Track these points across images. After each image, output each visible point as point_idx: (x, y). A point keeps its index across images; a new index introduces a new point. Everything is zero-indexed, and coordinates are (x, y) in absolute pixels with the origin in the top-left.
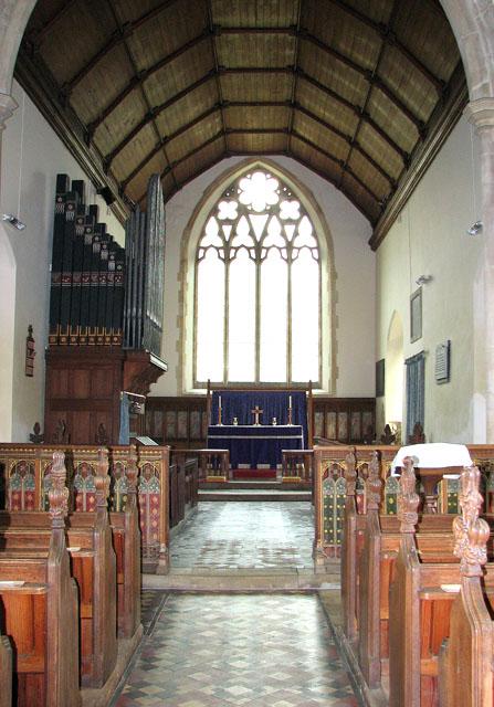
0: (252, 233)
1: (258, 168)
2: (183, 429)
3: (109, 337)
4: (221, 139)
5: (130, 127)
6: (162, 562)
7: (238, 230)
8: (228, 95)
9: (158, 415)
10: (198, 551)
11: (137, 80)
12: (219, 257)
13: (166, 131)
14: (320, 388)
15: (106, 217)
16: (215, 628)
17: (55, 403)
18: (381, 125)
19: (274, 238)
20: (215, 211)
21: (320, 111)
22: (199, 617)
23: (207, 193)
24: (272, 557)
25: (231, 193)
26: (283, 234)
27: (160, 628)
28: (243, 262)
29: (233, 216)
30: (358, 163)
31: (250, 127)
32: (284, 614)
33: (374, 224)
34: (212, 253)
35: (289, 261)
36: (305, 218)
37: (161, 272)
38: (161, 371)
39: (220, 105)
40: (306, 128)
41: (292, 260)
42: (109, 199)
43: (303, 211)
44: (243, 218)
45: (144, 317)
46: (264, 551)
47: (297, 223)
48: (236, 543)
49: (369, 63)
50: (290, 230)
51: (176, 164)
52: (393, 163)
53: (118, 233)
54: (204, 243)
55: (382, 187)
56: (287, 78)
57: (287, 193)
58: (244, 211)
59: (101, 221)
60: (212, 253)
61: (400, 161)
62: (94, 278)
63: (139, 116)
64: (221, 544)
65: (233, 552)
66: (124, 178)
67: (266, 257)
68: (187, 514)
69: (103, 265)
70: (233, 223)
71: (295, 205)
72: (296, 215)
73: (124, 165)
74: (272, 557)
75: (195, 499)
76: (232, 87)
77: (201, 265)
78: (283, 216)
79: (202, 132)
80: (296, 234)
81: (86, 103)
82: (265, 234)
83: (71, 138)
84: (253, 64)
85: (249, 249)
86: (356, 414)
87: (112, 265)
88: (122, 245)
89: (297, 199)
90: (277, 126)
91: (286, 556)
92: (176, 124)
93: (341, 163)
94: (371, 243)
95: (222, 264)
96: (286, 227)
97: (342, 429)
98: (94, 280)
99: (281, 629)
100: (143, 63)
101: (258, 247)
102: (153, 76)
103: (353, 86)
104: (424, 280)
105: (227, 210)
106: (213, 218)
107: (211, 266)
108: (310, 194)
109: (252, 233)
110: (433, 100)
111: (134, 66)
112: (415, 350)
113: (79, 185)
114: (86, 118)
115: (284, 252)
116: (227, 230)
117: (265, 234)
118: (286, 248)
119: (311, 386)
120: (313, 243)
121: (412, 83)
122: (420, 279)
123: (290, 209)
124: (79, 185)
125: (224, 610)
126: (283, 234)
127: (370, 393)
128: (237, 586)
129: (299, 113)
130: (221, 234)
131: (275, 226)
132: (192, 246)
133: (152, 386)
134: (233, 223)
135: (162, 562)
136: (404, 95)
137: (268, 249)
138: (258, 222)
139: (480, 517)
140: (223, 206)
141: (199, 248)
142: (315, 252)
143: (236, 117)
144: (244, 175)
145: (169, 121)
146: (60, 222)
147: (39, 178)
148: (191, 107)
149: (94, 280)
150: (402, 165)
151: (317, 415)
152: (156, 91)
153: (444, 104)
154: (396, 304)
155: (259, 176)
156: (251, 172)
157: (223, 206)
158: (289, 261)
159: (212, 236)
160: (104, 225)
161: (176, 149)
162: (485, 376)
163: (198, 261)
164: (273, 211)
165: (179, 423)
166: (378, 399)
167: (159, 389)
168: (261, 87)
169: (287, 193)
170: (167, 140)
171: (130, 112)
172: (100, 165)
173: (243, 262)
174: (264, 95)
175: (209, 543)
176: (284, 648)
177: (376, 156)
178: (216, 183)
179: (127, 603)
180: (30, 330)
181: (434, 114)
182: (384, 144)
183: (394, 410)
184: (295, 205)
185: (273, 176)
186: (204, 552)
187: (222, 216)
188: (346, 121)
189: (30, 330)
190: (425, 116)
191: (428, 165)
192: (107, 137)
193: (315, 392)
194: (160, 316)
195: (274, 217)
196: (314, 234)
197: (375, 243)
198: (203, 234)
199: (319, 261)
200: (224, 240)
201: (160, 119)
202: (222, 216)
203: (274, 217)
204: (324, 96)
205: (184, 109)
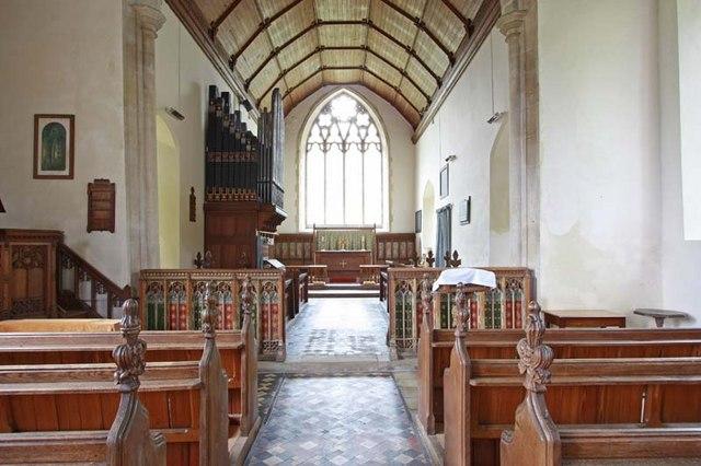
1: (343, 93)
2: (299, 253)
3: (249, 195)
4: (320, 73)
5: (261, 62)
6: (280, 353)
7: (331, 132)
8: (324, 42)
9: (285, 245)
10: (307, 338)
11: (264, 25)
13: (285, 66)
15: (245, 117)
16: (318, 413)
17: (209, 240)
18: (423, 58)
19: (354, 138)
20: (317, 120)
21: (383, 53)
22: (303, 395)
23: (312, 109)
24: (358, 345)
25: (326, 109)
26: (359, 135)
27: (275, 415)
28: (335, 151)
29: (328, 123)
30: (407, 88)
31: (338, 65)
32: (370, 398)
34: (316, 147)
36: (372, 125)
37: (280, 157)
38: (284, 218)
39: (320, 49)
40: (374, 65)
42: (248, 108)
43: (371, 120)
44: (334, 125)
45: (271, 182)
46: (352, 338)
47: (367, 128)
48: (333, 332)
49: (417, 13)
51: (292, 89)
52: (429, 85)
53: (253, 128)
54: (311, 140)
55: (420, 102)
56: (362, 28)
57: (361, 109)
58: (335, 120)
59: (242, 121)
60: (316, 147)
61: (435, 84)
62: (237, 156)
63: (267, 54)
64: (323, 332)
65: (331, 340)
66: (259, 97)
68: (301, 309)
69: (242, 148)
70: (329, 128)
71: (366, 116)
72: (367, 123)
73: (258, 88)
74: (358, 345)
75: (306, 297)
76: (327, 35)
77: (309, 154)
78: (359, 123)
79: (308, 68)
80: (367, 135)
81: (229, 42)
82: (348, 135)
83: (218, 61)
84: (340, 19)
86: (389, 243)
87: (248, 147)
88: (255, 134)
89: (366, 111)
90: (356, 65)
91: (368, 343)
92: (292, 61)
93: (395, 88)
94: (412, 139)
95: (322, 153)
97: (395, 252)
98: (237, 157)
99: (369, 415)
100: (267, 13)
102: (274, 23)
103: (406, 32)
104: (453, 158)
105: (325, 120)
106: (316, 125)
107: (315, 152)
108: (376, 110)
110: (462, 34)
111: (261, 15)
112: (440, 204)
113: (226, 95)
114: (231, 51)
115: (360, 146)
116: (325, 132)
117: (348, 135)
120: (377, 140)
121: (447, 23)
123: (363, 119)
124: (226, 95)
125: (324, 394)
129: (369, 54)
132: (303, 143)
133: (278, 227)
134: (329, 128)
135: (280, 353)
136: (439, 33)
138: (344, 128)
140: (322, 117)
141: (307, 144)
143: (330, 58)
144: (335, 97)
145: (287, 58)
146: (211, 117)
147: (196, 88)
148: (300, 49)
149: (237, 157)
150: (436, 86)
152: (277, 34)
153: (470, 36)
154: (428, 172)
155: (343, 98)
156: (338, 96)
157: (322, 117)
159: (316, 138)
160: (245, 124)
161: (292, 79)
162: (73, 327)
163: (307, 151)
164: (353, 120)
165: (297, 249)
166: (417, 235)
167: (281, 229)
168: (346, 36)
169: (361, 109)
170: (279, 50)
171: (259, 50)
172: (242, 87)
173: (335, 151)
174: (348, 42)
175: (315, 332)
176: (374, 438)
177: (419, 82)
178: (317, 102)
179: (246, 382)
180: (193, 190)
181: (462, 46)
182: (424, 72)
183: (428, 241)
184: (366, 116)
185: (353, 98)
186: (311, 340)
187: (321, 123)
188: (399, 57)
189: (193, 190)
190: (454, 48)
191: (455, 82)
192: (246, 66)
194: (281, 178)
196: (378, 135)
197: (415, 140)
198: (310, 135)
199: (381, 151)
201: (280, 56)
202: (321, 123)
204: (386, 40)
205: (296, 50)
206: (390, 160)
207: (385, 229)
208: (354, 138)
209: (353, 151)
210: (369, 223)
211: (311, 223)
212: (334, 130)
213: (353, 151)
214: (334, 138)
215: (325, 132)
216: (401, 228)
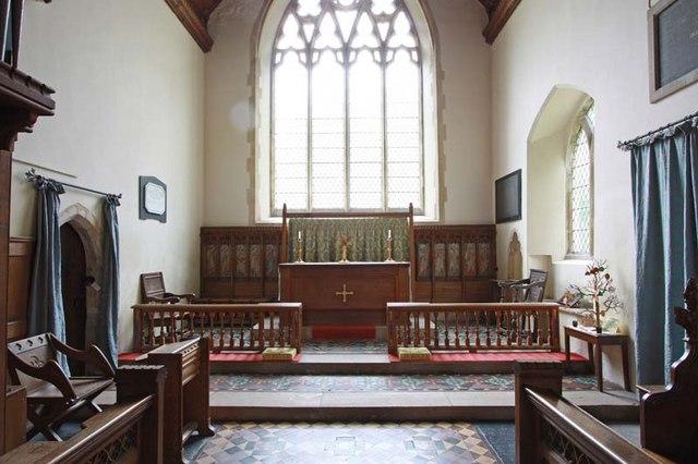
0: (338, 32)
12: (300, 61)
14: (422, 214)
28: (328, 64)
33: (491, 10)
34: (402, 55)
35: (384, 64)
36: (402, 15)
41: (312, 64)
44: (328, 15)
47: (391, 19)
50: (383, 28)
54: (281, 45)
67: (354, 61)
70: (315, 20)
82: (354, 32)
85: (335, 51)
96: (380, 25)
101: (346, 49)
109: (338, 32)
115: (340, 55)
116: (383, 28)
117: (354, 32)
118: (341, 50)
119: (411, 212)
120: (411, 42)
122: (601, 391)
126: (376, 32)
127: (517, 213)
128: (297, 417)
130: (376, 32)
131: (365, 23)
134: (315, 20)
137: (395, 50)
139: (635, 147)
142: (415, 54)
151: (422, 246)
158: (384, 64)
159: (291, 37)
173: (328, 64)
193: (417, 219)
195: (365, 15)
196: (414, 31)
198: (279, 33)
199: (420, 63)
200: (305, 40)
203: (365, 15)
206: (440, 76)
207: (430, 216)
208: (365, 37)
209: (365, 63)
210: (398, 203)
211: (279, 206)
212: (327, 23)
213: (365, 63)
214: (327, 39)
215: (309, 29)
216: (464, 213)
